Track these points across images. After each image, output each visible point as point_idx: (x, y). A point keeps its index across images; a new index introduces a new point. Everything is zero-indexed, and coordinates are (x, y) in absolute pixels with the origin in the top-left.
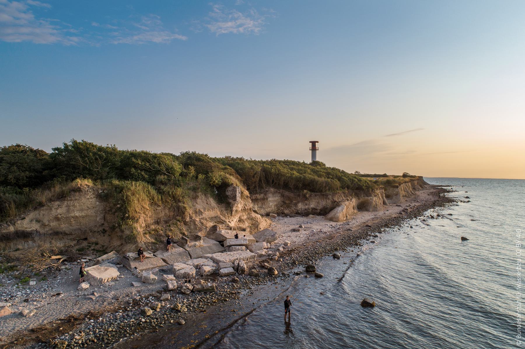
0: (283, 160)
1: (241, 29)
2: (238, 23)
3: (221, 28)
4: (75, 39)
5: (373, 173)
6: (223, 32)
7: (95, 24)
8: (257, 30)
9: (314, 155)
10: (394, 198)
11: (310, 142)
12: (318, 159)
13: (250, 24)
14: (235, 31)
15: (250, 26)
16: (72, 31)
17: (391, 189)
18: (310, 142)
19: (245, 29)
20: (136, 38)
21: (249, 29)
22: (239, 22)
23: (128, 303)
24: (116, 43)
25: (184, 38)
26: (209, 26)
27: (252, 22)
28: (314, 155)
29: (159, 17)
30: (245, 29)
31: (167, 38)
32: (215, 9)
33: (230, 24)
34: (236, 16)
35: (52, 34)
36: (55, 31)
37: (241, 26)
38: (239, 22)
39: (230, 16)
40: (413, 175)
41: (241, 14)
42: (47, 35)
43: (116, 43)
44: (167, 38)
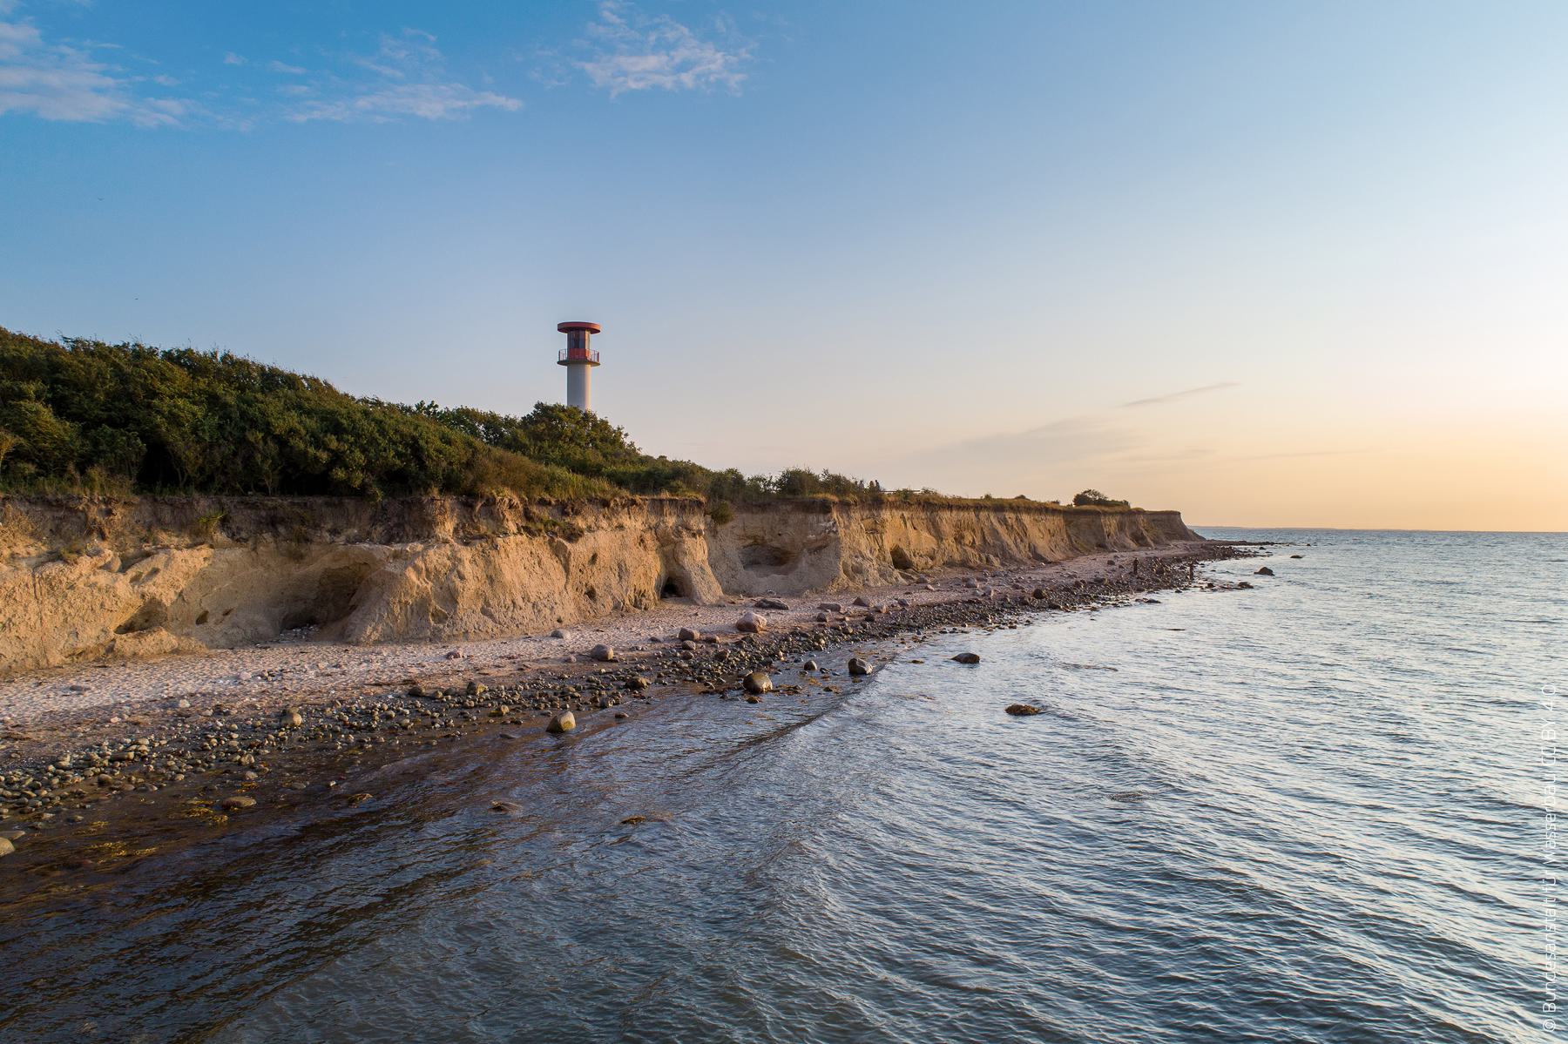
0: (287, 371)
1: (687, 79)
2: (677, 60)
3: (625, 74)
4: (173, 105)
5: (975, 493)
6: (633, 85)
7: (232, 59)
8: (735, 79)
9: (576, 387)
10: (803, 564)
11: (564, 328)
12: (598, 404)
13: (714, 60)
14: (668, 82)
15: (713, 67)
16: (162, 80)
17: (796, 517)
18: (564, 328)
19: (698, 77)
20: (363, 103)
21: (712, 79)
22: (681, 55)
23: (809, 796)
24: (301, 119)
25: (513, 104)
26: (589, 67)
27: (719, 55)
28: (576, 387)
29: (432, 38)
30: (698, 77)
31: (460, 103)
32: (606, 14)
33: (652, 62)
34: (670, 36)
35: (99, 91)
36: (110, 82)
37: (684, 67)
38: (681, 55)
39: (653, 38)
40: (1119, 499)
41: (685, 30)
42: (83, 93)
43: (301, 119)
44: (460, 103)
